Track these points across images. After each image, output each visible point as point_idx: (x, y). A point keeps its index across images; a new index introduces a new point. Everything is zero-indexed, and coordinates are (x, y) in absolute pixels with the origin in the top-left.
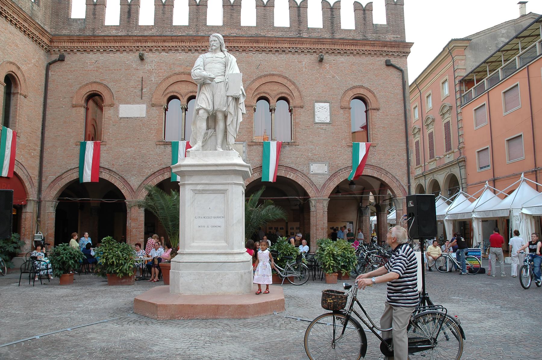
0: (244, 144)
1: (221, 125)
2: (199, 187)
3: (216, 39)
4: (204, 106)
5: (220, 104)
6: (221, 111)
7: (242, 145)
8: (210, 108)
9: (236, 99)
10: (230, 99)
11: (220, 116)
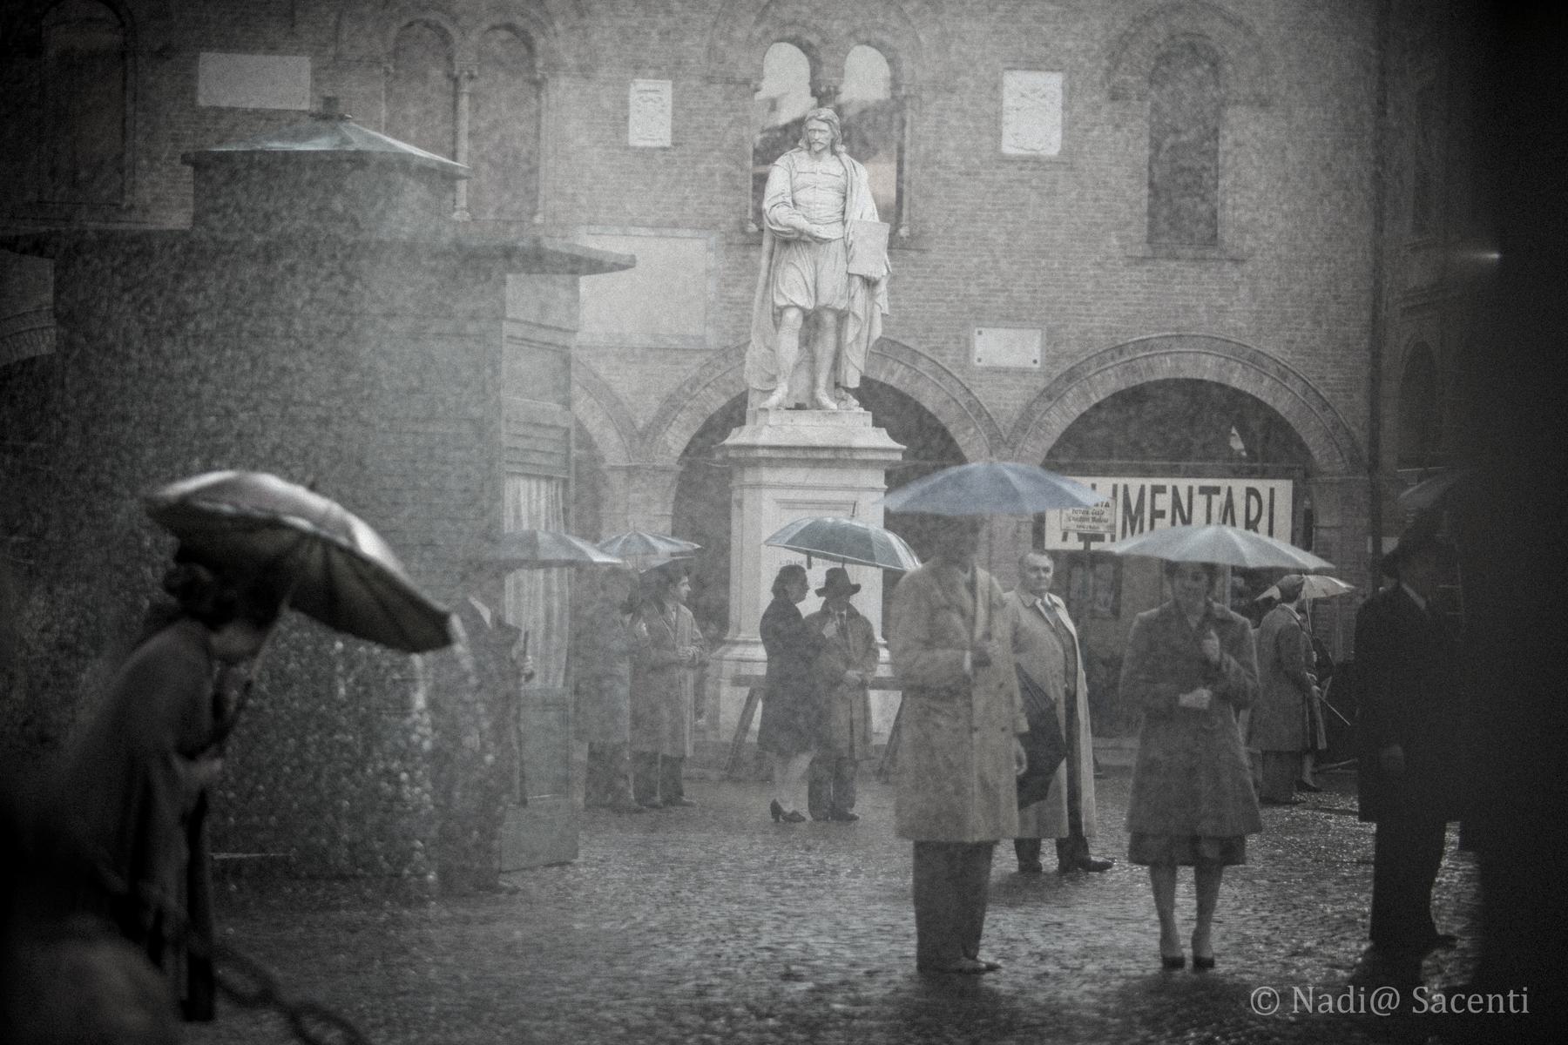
0: (713, 240)
1: (830, 339)
2: (792, 495)
3: (825, 126)
4: (801, 303)
5: (832, 289)
6: (834, 310)
7: (699, 244)
8: (810, 307)
9: (870, 283)
10: (857, 281)
11: (829, 319)
